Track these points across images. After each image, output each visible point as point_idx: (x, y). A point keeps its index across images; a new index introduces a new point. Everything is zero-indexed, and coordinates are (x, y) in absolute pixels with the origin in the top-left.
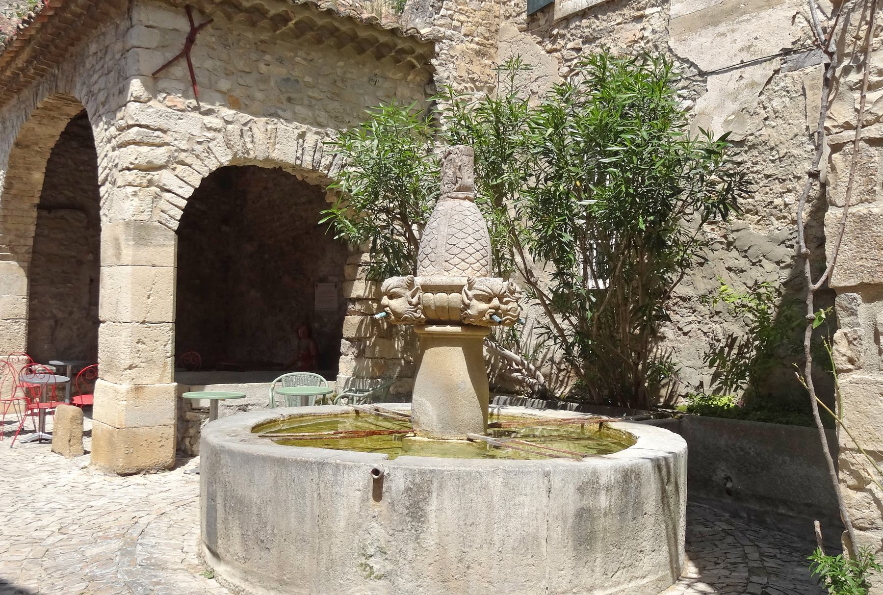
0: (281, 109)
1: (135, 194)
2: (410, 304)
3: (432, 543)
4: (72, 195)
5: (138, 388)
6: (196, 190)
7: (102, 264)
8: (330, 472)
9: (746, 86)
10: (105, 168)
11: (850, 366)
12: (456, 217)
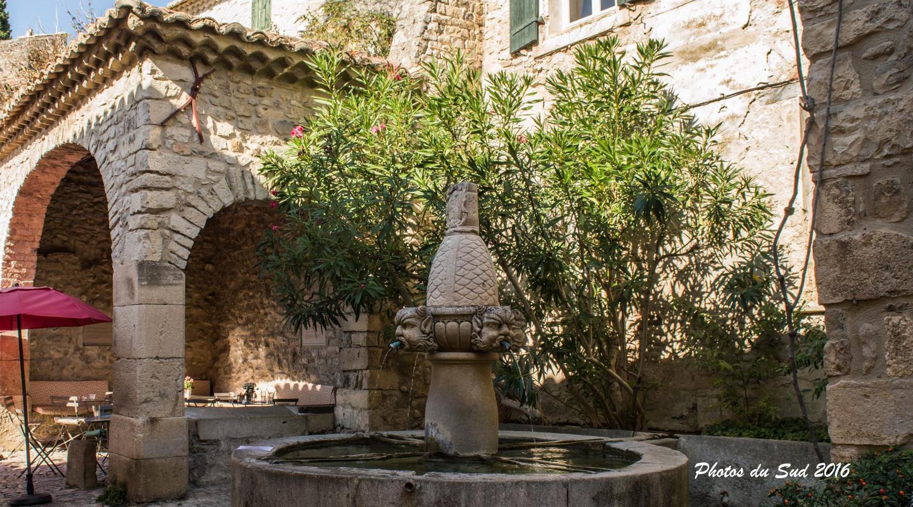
1: (147, 237)
2: (423, 332)
4: (66, 239)
5: (153, 421)
6: (201, 230)
7: (114, 304)
8: (365, 487)
9: (728, 118)
10: (116, 212)
11: (838, 373)
12: (463, 250)
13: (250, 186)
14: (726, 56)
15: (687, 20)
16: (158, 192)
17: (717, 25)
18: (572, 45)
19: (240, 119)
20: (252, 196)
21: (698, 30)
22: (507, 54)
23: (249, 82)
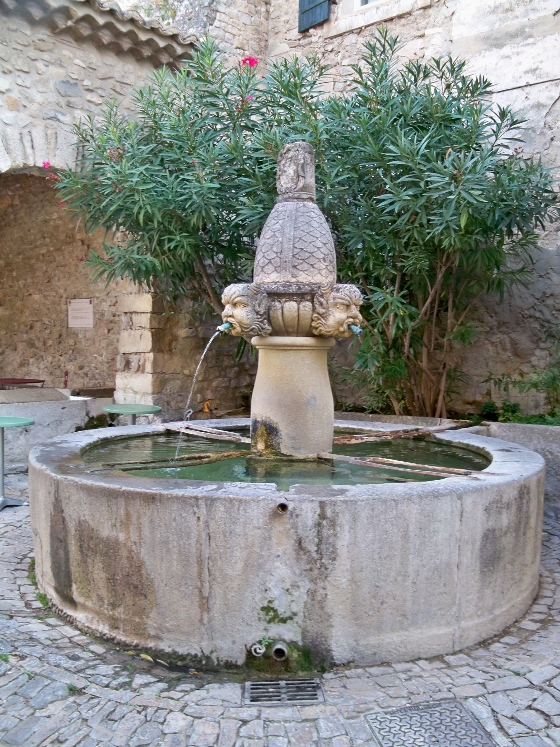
0: (61, 112)
2: (257, 313)
3: (344, 580)
8: (222, 509)
9: (532, 107)
13: (29, 151)
14: (534, 44)
15: (492, 5)
17: (526, 11)
18: (366, 27)
19: (18, 73)
20: (31, 163)
21: (505, 15)
22: (295, 34)
23: (28, 32)
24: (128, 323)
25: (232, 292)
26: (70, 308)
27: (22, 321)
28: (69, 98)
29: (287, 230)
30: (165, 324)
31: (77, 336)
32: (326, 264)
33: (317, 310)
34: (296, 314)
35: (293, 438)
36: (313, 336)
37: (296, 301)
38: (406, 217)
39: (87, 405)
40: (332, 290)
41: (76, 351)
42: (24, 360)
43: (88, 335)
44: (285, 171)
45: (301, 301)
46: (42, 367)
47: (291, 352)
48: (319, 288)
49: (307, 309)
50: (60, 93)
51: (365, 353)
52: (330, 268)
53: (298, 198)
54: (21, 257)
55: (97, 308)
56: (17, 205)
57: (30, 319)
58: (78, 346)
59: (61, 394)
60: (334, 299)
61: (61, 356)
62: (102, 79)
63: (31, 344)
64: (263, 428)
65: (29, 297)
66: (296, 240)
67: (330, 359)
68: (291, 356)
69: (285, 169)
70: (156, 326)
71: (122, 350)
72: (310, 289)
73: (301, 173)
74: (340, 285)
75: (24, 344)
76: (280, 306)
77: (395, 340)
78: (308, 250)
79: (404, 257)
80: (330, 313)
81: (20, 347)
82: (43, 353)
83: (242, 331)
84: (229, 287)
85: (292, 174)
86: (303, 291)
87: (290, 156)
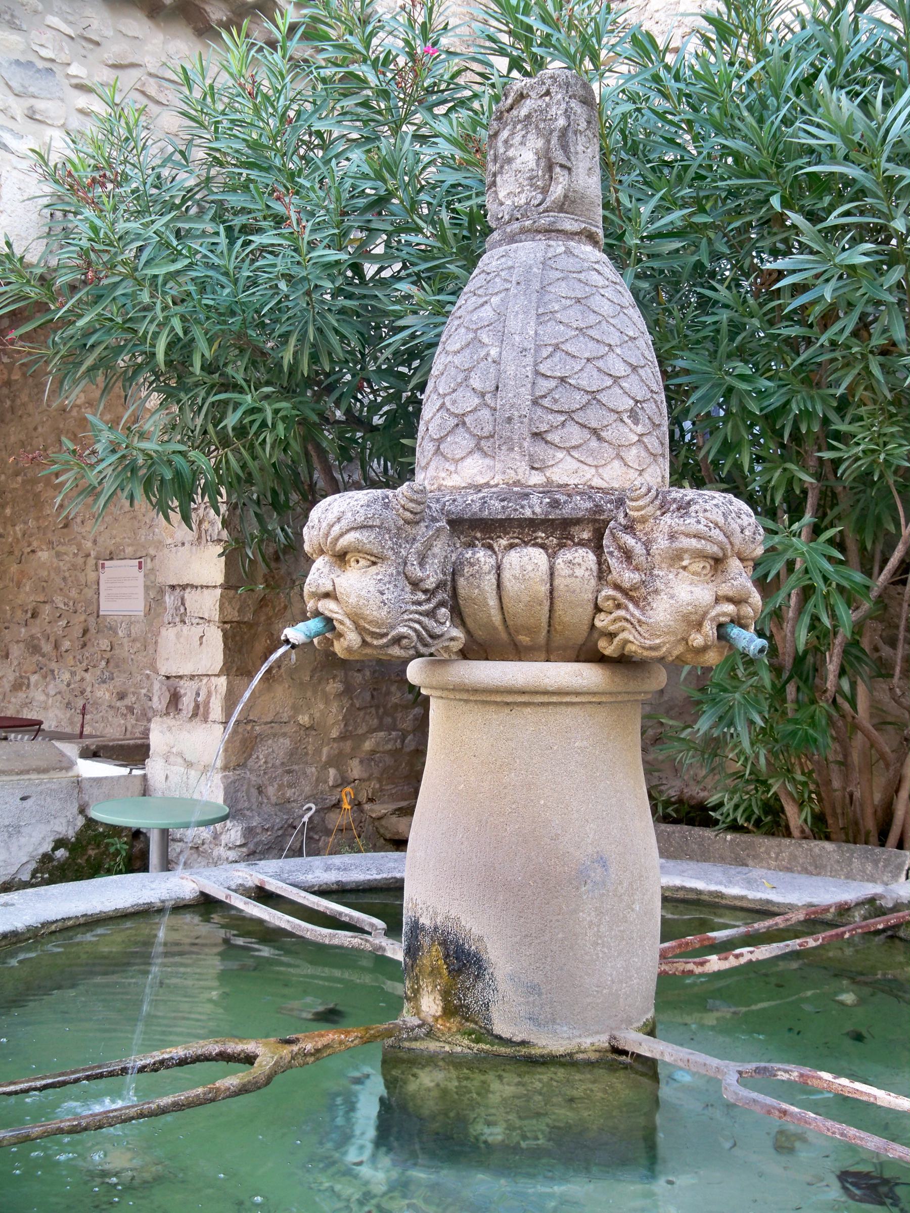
2: (415, 585)
16: (495, 587)
24: (177, 609)
25: (331, 517)
26: (103, 578)
27: (20, 602)
28: (32, 101)
29: (513, 324)
30: (255, 613)
31: (116, 633)
32: (639, 429)
33: (614, 576)
34: (544, 589)
35: (533, 989)
36: (600, 659)
37: (543, 546)
38: (849, 322)
39: (80, 791)
40: (664, 508)
41: (112, 662)
42: (21, 677)
43: (136, 630)
44: (509, 161)
45: (561, 546)
46: (52, 693)
47: (529, 710)
48: (620, 502)
49: (579, 572)
50: (10, 87)
51: (725, 690)
52: (652, 442)
53: (550, 231)
54: (19, 479)
55: (152, 578)
56: (16, 381)
57: (32, 598)
58: (117, 651)
59: (62, 754)
60: (672, 537)
61: (86, 670)
62: (115, 66)
63: (34, 649)
64: (437, 951)
65: (32, 556)
66: (545, 353)
67: (653, 740)
68: (527, 724)
69: (511, 153)
70: (234, 615)
71: (166, 667)
72: (589, 505)
73: (559, 156)
74: (689, 493)
75: (22, 645)
76: (492, 561)
77: (799, 660)
78: (584, 383)
79: (838, 436)
80: (659, 584)
81: (16, 651)
82: (53, 665)
83: (365, 643)
84: (323, 504)
85: (532, 164)
86: (566, 512)
87: (524, 112)
